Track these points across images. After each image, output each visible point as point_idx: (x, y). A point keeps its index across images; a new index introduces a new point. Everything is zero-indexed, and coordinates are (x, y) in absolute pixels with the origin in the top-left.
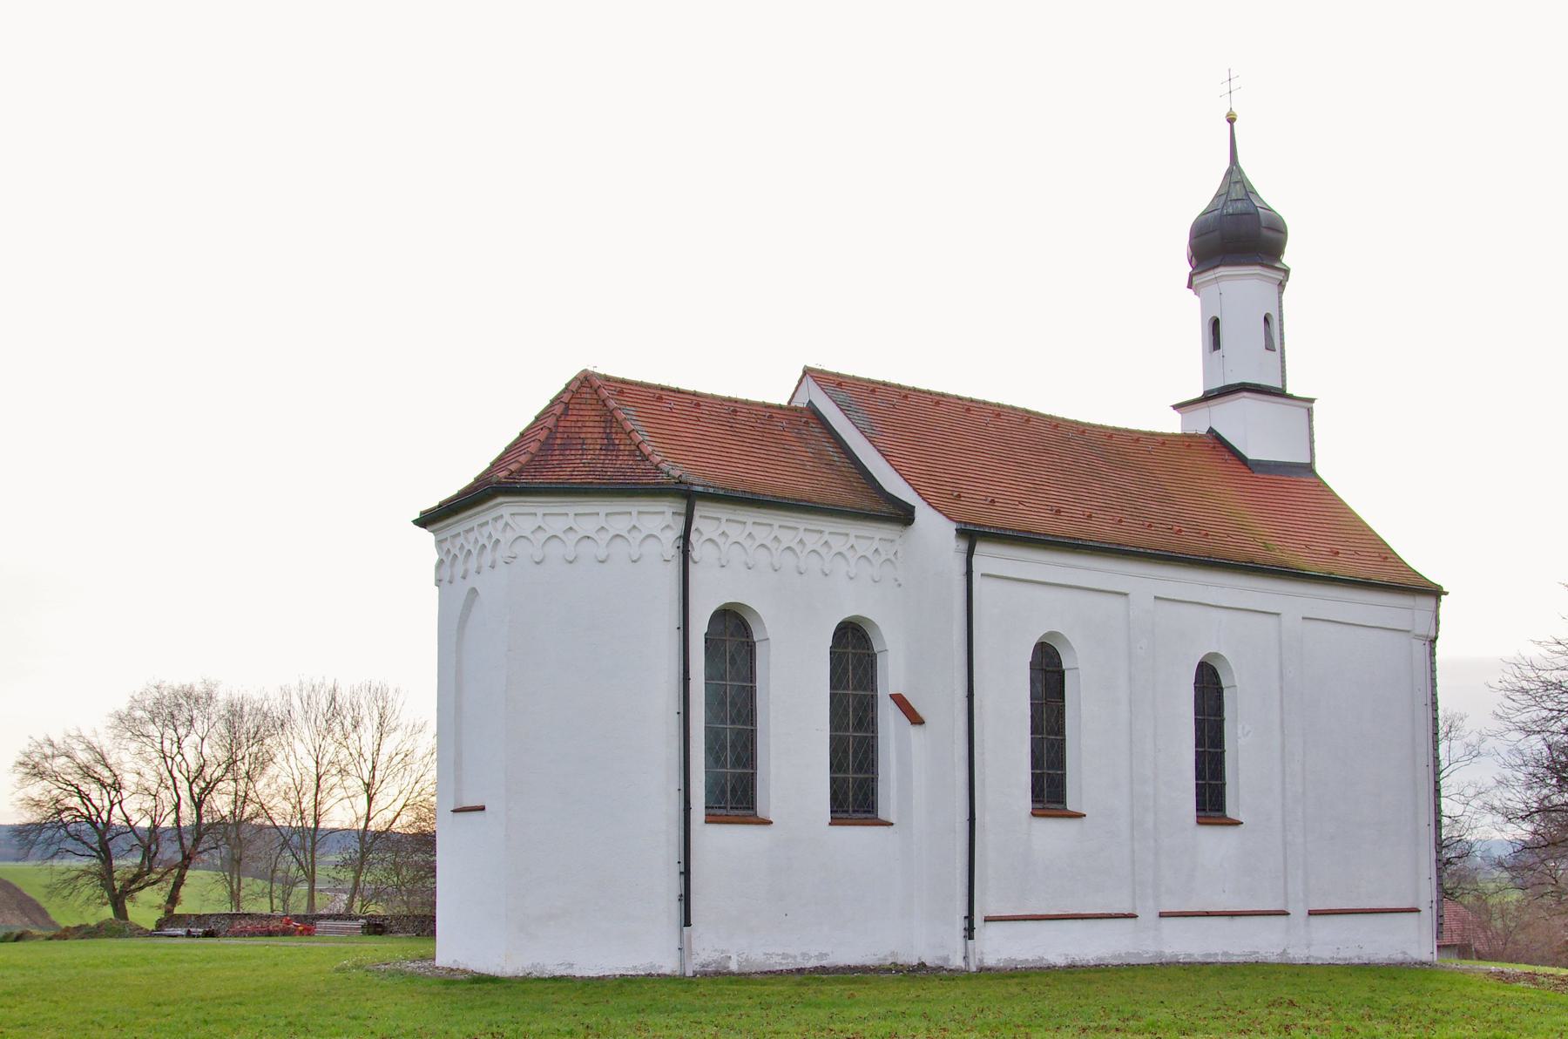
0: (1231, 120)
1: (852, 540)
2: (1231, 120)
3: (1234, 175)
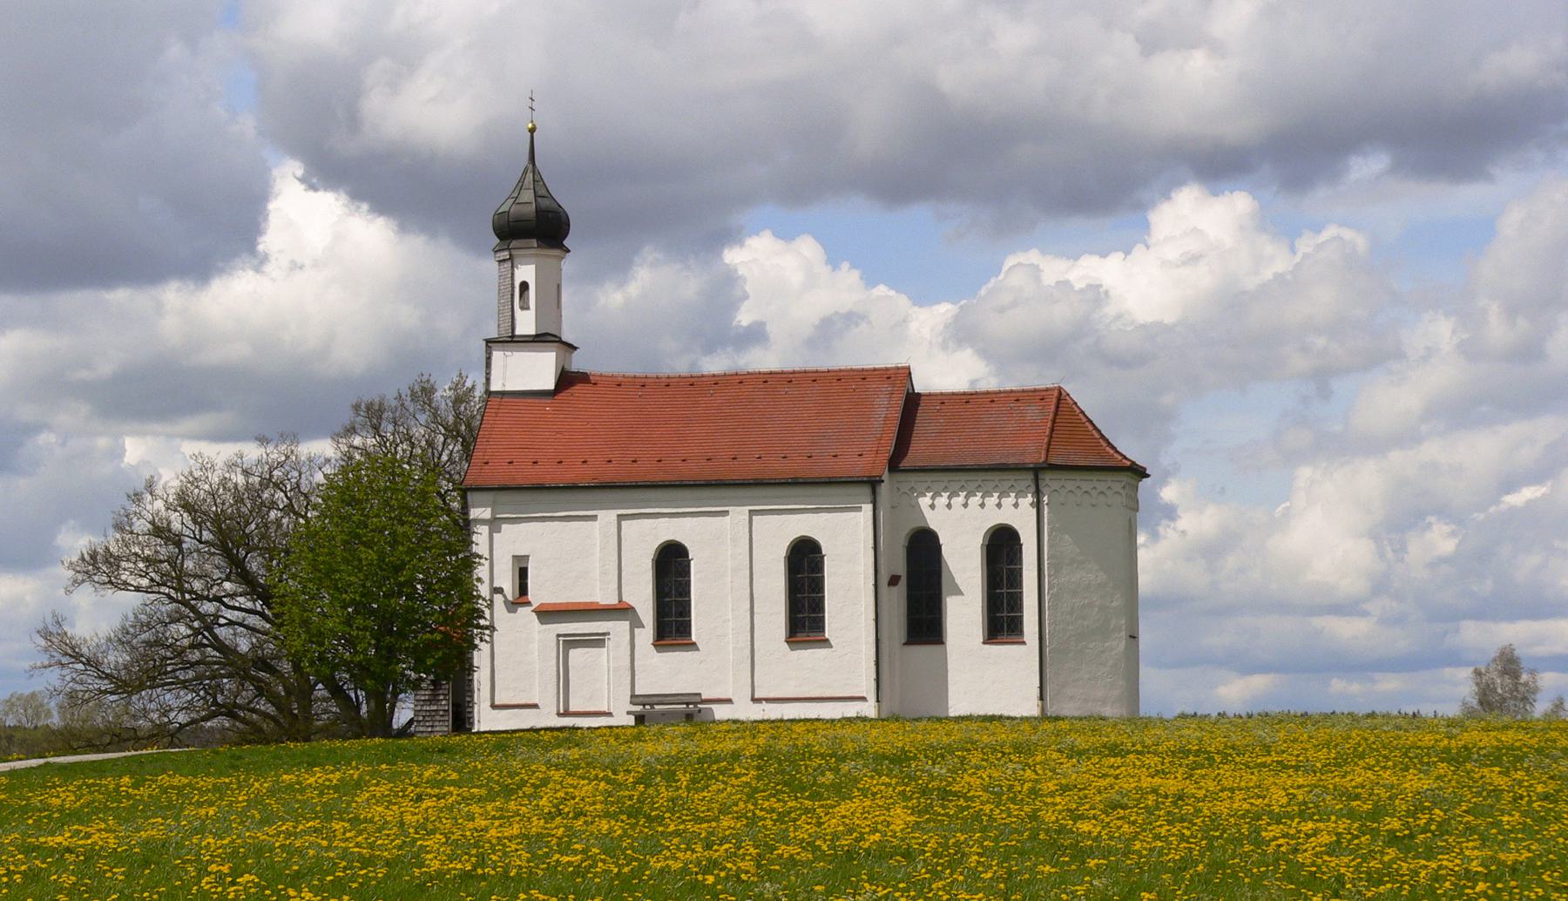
0: (532, 131)
1: (963, 483)
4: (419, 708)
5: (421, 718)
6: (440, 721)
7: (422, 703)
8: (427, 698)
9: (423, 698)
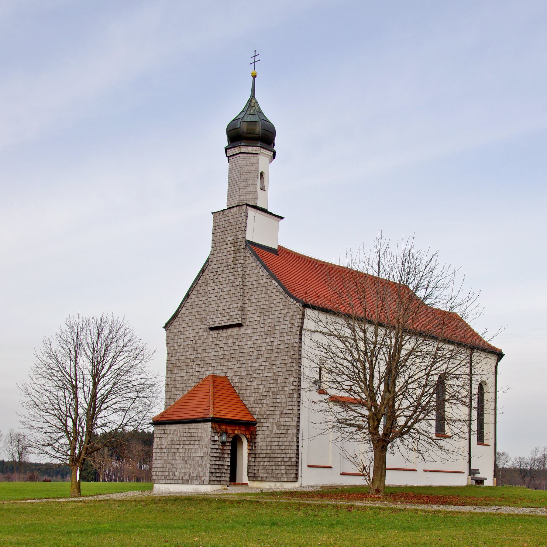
0: (254, 77)
2: (254, 77)
3: (252, 103)
4: (212, 463)
5: (214, 471)
6: (225, 473)
7: (214, 459)
8: (218, 455)
9: (215, 455)
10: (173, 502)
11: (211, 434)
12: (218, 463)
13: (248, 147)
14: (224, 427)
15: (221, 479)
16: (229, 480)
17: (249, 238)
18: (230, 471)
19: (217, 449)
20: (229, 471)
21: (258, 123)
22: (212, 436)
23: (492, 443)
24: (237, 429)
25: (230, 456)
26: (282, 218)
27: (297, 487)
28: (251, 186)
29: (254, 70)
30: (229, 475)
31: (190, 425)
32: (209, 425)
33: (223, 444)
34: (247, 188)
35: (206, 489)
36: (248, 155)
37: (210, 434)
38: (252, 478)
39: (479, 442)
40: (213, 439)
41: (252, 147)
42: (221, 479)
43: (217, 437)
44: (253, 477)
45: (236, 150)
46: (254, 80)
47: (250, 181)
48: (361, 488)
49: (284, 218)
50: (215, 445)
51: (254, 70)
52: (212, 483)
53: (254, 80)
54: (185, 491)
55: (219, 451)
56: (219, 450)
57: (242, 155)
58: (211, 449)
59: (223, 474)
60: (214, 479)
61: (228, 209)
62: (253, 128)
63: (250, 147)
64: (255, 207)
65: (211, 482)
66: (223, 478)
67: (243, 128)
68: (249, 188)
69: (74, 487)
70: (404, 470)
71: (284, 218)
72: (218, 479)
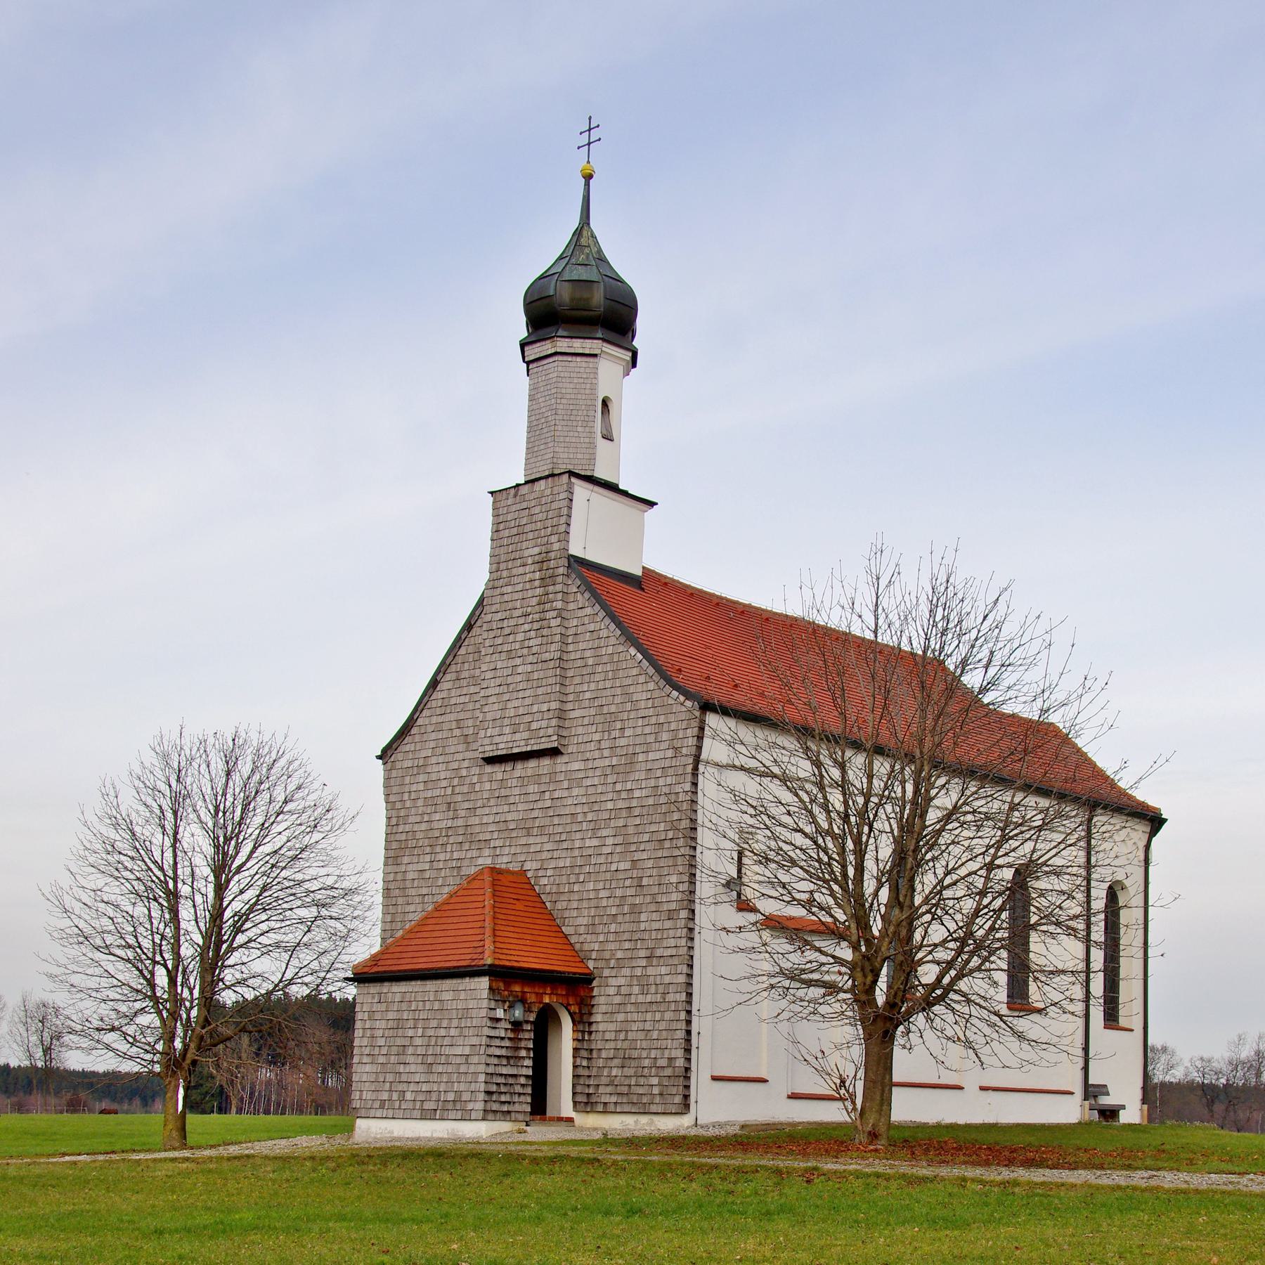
0: (588, 178)
2: (588, 178)
3: (582, 238)
4: (491, 1070)
5: (494, 1088)
6: (520, 1094)
7: (496, 1061)
8: (503, 1052)
9: (498, 1052)
10: (399, 1160)
11: (489, 1004)
12: (505, 1071)
13: (574, 340)
14: (517, 988)
15: (511, 1108)
16: (529, 1109)
17: (575, 550)
18: (532, 1090)
19: (502, 1038)
20: (529, 1090)
21: (596, 284)
22: (491, 1009)
23: (1137, 1024)
24: (548, 991)
25: (532, 1055)
26: (652, 504)
27: (686, 1125)
28: (580, 429)
29: (588, 162)
30: (529, 1099)
31: (439, 982)
32: (484, 982)
33: (517, 1026)
34: (571, 434)
35: (477, 1130)
36: (574, 358)
37: (485, 1004)
38: (582, 1104)
39: (1107, 1023)
40: (492, 1014)
41: (582, 340)
42: (511, 1108)
43: (502, 1010)
44: (585, 1102)
45: (546, 348)
46: (587, 185)
47: (578, 418)
48: (834, 1129)
49: (656, 504)
50: (498, 1030)
51: (588, 162)
52: (490, 1116)
53: (587, 185)
54: (428, 1134)
55: (507, 1043)
56: (507, 1040)
57: (560, 358)
58: (488, 1039)
59: (517, 1095)
60: (495, 1107)
61: (527, 482)
62: (585, 295)
63: (579, 340)
64: (591, 480)
65: (487, 1114)
66: (517, 1105)
67: (561, 296)
68: (576, 434)
69: (170, 1127)
70: (934, 1088)
71: (656, 504)
72: (505, 1108)
